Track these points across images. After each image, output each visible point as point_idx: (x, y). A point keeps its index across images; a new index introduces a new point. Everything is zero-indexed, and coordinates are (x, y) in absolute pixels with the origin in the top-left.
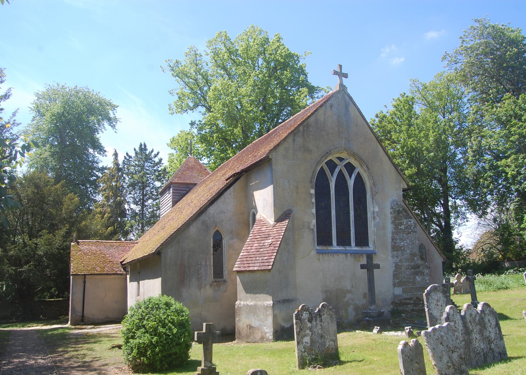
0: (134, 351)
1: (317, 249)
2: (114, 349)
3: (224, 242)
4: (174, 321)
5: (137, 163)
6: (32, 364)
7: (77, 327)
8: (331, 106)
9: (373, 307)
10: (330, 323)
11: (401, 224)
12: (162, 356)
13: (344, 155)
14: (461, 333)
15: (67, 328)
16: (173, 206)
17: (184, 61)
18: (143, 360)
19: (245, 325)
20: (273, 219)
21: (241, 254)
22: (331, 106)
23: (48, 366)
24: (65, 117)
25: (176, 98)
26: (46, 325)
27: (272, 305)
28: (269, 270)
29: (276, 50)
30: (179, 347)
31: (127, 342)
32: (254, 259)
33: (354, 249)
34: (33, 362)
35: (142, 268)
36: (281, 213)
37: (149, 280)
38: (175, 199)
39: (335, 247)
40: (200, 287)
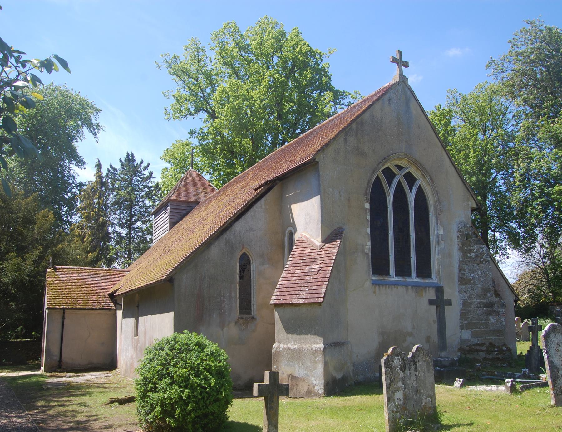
0: (156, 410)
1: (372, 280)
2: (113, 405)
3: (253, 268)
4: (210, 368)
5: (122, 176)
6: (5, 424)
7: (53, 374)
8: (390, 100)
9: (443, 354)
10: (426, 373)
11: (470, 251)
12: (196, 417)
15: (41, 376)
16: (170, 229)
17: (185, 57)
18: (170, 422)
19: (285, 375)
20: (320, 239)
21: (279, 283)
22: (390, 100)
23: (28, 427)
24: (37, 120)
25: (173, 101)
26: (13, 371)
27: (322, 349)
28: (320, 303)
29: (295, 47)
30: (218, 403)
31: (144, 396)
32: (298, 289)
33: (415, 280)
34: (6, 421)
35: (141, 302)
36: (330, 231)
37: (153, 316)
38: (173, 221)
39: (393, 277)
40: (222, 325)
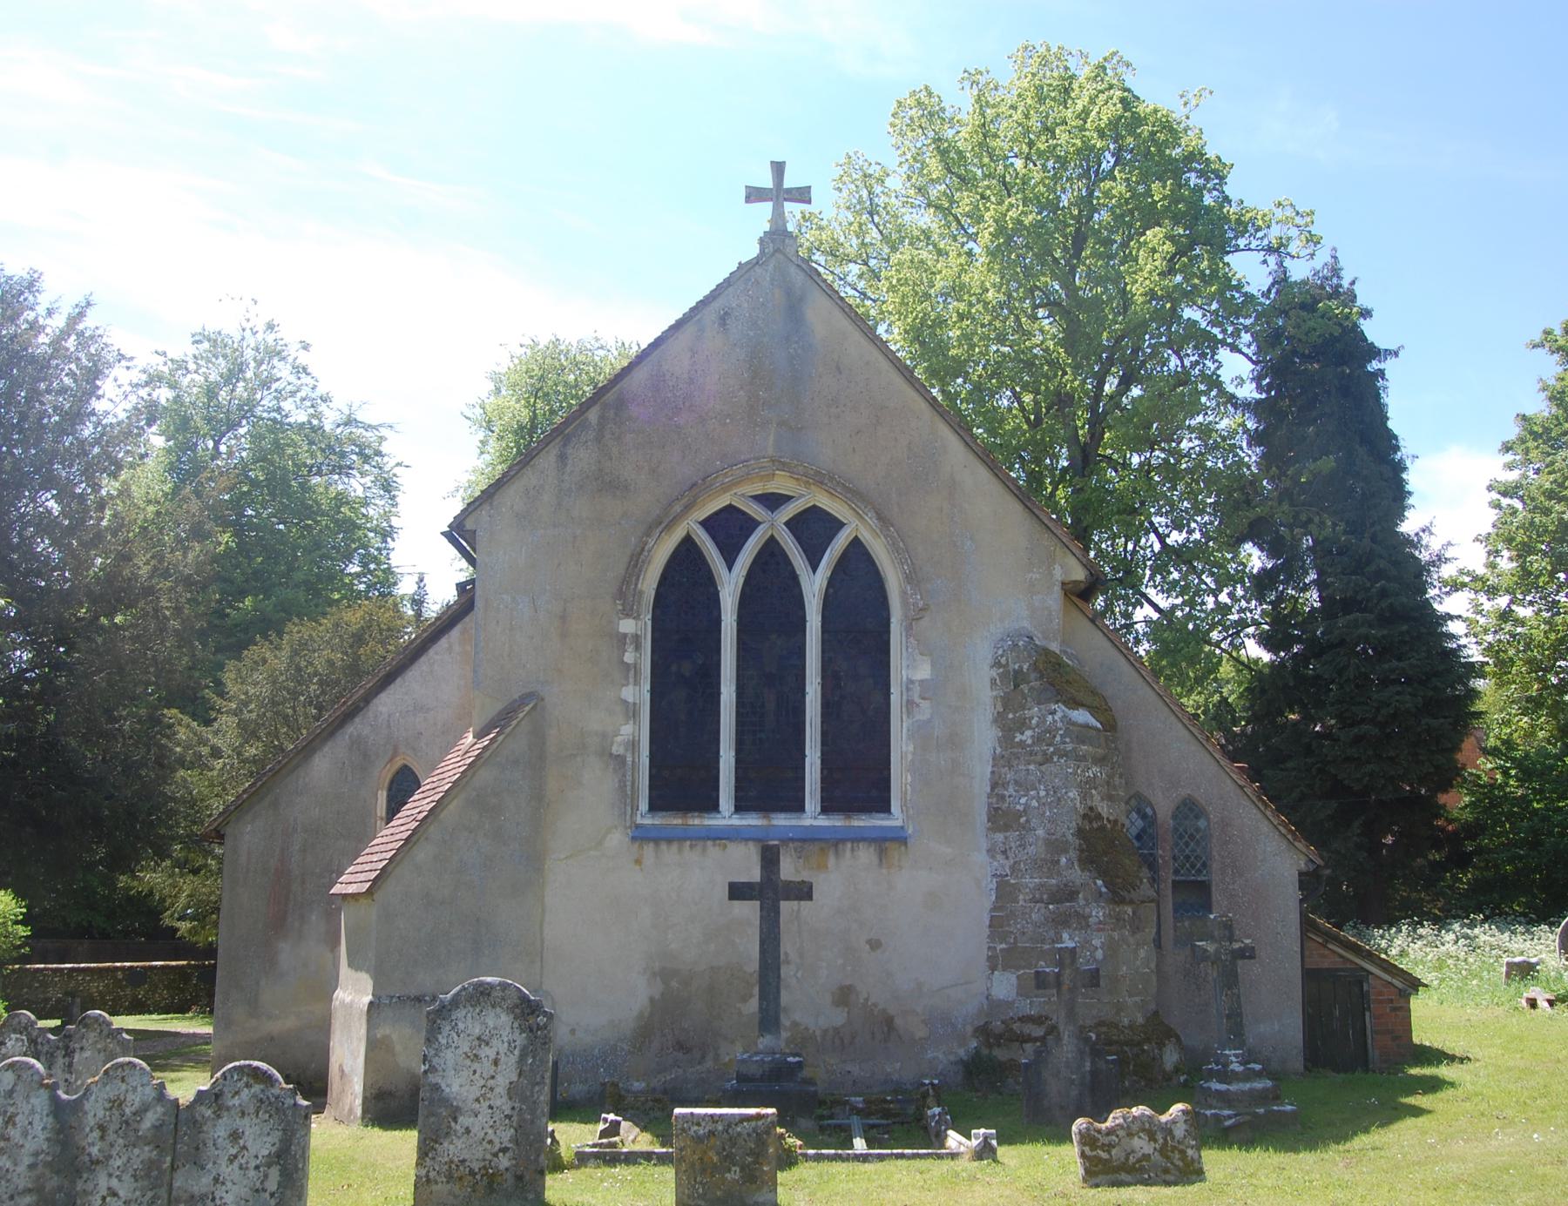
11: (1022, 725)
13: (780, 484)
14: (27, 1161)
39: (726, 815)
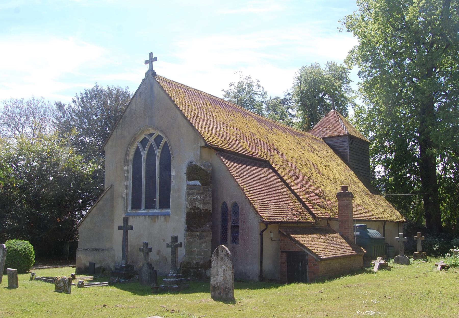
13: (152, 131)
